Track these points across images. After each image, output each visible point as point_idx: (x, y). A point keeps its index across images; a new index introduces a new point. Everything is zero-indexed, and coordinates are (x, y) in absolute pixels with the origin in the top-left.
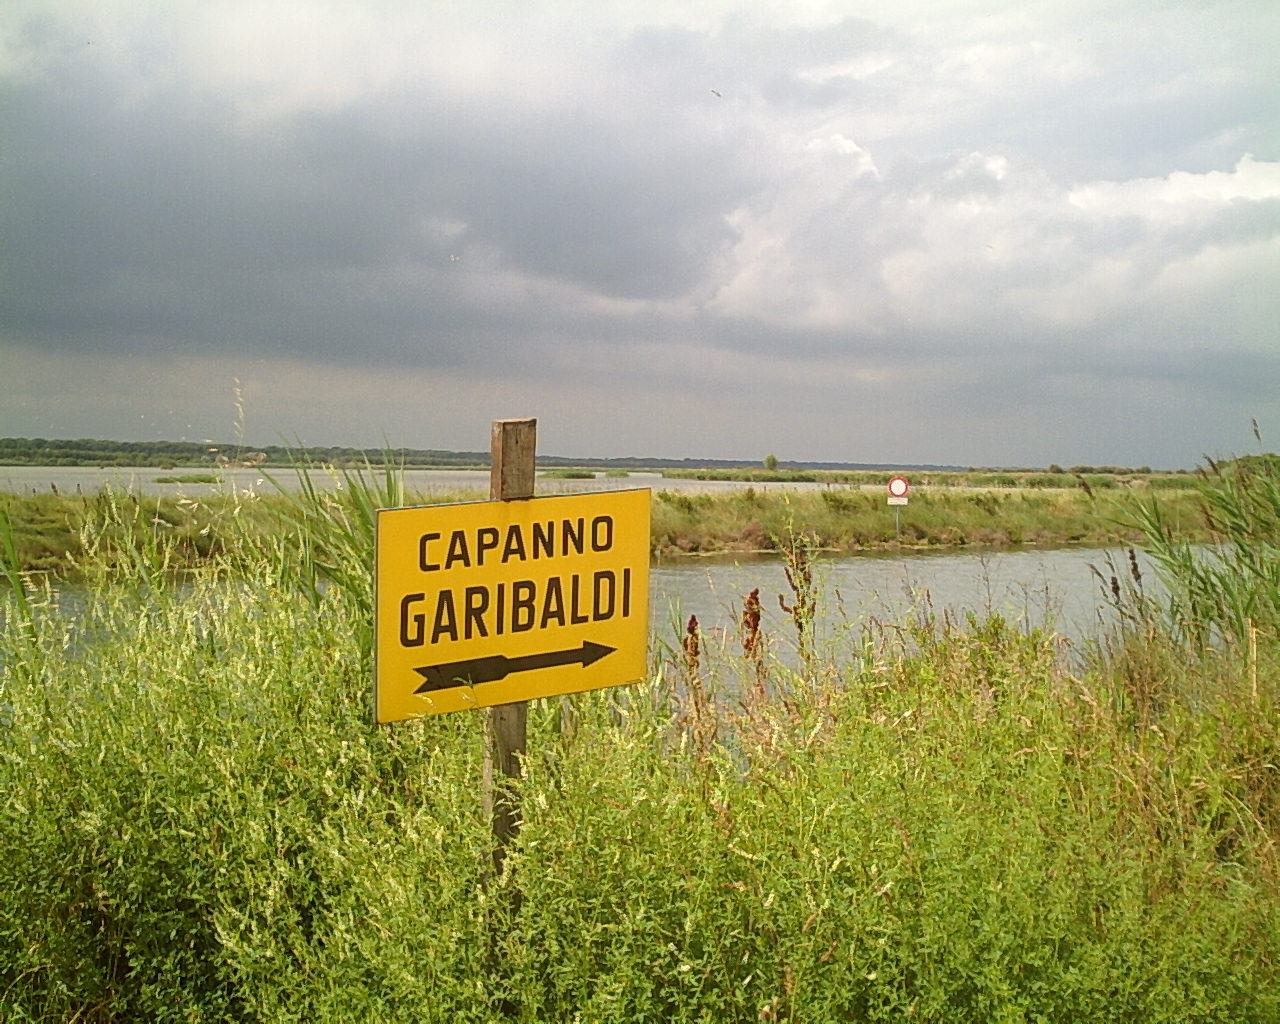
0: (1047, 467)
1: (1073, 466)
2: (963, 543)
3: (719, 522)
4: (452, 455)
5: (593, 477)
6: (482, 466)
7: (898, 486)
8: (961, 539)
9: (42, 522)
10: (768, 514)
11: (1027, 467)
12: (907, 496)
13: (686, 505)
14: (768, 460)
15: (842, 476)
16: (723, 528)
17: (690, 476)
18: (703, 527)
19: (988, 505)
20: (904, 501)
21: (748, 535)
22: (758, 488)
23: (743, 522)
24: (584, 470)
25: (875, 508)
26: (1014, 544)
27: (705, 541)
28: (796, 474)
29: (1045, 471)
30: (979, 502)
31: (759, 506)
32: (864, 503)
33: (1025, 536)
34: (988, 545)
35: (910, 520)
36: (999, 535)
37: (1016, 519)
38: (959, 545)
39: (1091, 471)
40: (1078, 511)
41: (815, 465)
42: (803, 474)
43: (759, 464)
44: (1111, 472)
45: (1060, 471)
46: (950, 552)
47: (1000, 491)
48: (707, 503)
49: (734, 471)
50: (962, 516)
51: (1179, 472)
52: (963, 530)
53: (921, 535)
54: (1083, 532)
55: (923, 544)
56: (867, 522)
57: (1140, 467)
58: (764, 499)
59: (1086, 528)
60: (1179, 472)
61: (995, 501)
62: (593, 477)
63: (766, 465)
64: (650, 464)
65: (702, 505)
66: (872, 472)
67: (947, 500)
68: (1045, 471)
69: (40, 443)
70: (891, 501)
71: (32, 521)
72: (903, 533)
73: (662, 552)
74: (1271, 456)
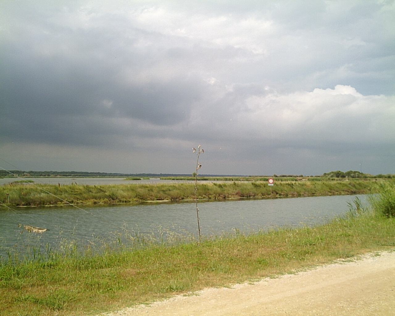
0: (273, 175)
1: (280, 175)
2: (287, 195)
3: (229, 190)
4: (88, 173)
5: (141, 180)
6: (98, 177)
7: (271, 181)
8: (287, 194)
9: (75, 192)
10: (240, 188)
11: (266, 175)
12: (273, 183)
13: (220, 186)
14: (194, 174)
15: (216, 179)
16: (230, 192)
17: (170, 179)
18: (225, 192)
19: (291, 185)
20: (273, 185)
21: (237, 194)
22: (236, 182)
23: (235, 190)
24: (138, 178)
25: (265, 187)
26: (299, 195)
27: (227, 195)
28: (203, 178)
29: (272, 177)
30: (289, 185)
31: (238, 187)
32: (262, 186)
33: (302, 193)
34: (293, 196)
35: (274, 190)
36: (296, 193)
37: (299, 189)
38: (286, 196)
39: (285, 176)
40: (313, 187)
41: (209, 176)
42: (204, 178)
43: (191, 175)
44: (291, 176)
45: (276, 176)
46: (284, 198)
47: (294, 182)
48: (225, 186)
49: (183, 177)
50: (286, 188)
51: (311, 176)
52: (287, 192)
53: (277, 194)
54: (315, 192)
55: (278, 196)
56: (263, 190)
57: (300, 175)
58: (238, 184)
59: (316, 191)
60: (311, 176)
61: (293, 184)
62: (141, 180)
63: (193, 175)
64: (121, 175)
65: (224, 186)
66: (225, 177)
67: (281, 184)
68: (272, 177)
69: (111, 174)
70: (269, 185)
71: (72, 192)
72: (272, 193)
73: (218, 198)
74: (340, 171)
